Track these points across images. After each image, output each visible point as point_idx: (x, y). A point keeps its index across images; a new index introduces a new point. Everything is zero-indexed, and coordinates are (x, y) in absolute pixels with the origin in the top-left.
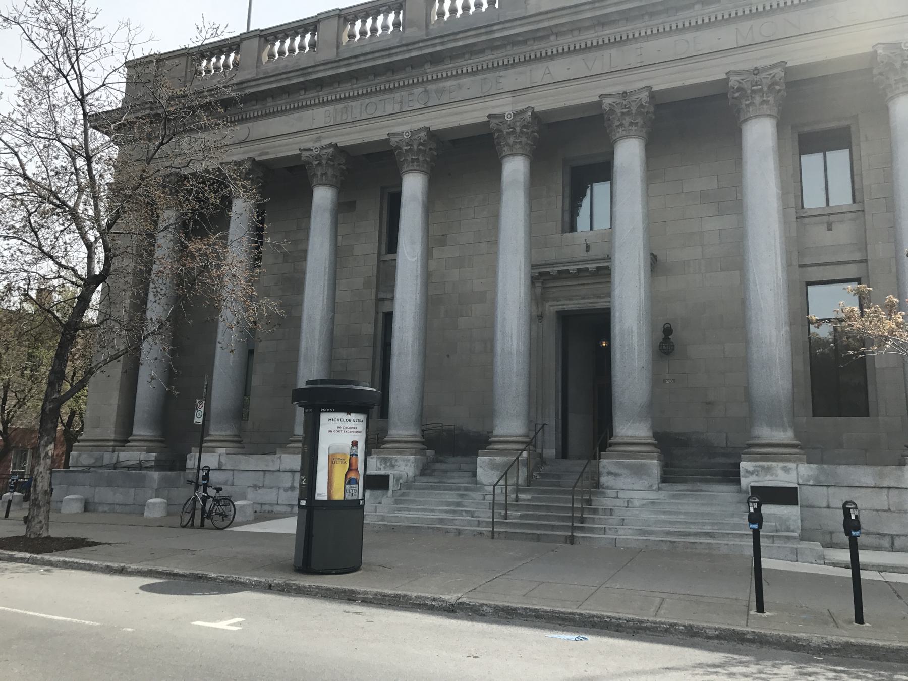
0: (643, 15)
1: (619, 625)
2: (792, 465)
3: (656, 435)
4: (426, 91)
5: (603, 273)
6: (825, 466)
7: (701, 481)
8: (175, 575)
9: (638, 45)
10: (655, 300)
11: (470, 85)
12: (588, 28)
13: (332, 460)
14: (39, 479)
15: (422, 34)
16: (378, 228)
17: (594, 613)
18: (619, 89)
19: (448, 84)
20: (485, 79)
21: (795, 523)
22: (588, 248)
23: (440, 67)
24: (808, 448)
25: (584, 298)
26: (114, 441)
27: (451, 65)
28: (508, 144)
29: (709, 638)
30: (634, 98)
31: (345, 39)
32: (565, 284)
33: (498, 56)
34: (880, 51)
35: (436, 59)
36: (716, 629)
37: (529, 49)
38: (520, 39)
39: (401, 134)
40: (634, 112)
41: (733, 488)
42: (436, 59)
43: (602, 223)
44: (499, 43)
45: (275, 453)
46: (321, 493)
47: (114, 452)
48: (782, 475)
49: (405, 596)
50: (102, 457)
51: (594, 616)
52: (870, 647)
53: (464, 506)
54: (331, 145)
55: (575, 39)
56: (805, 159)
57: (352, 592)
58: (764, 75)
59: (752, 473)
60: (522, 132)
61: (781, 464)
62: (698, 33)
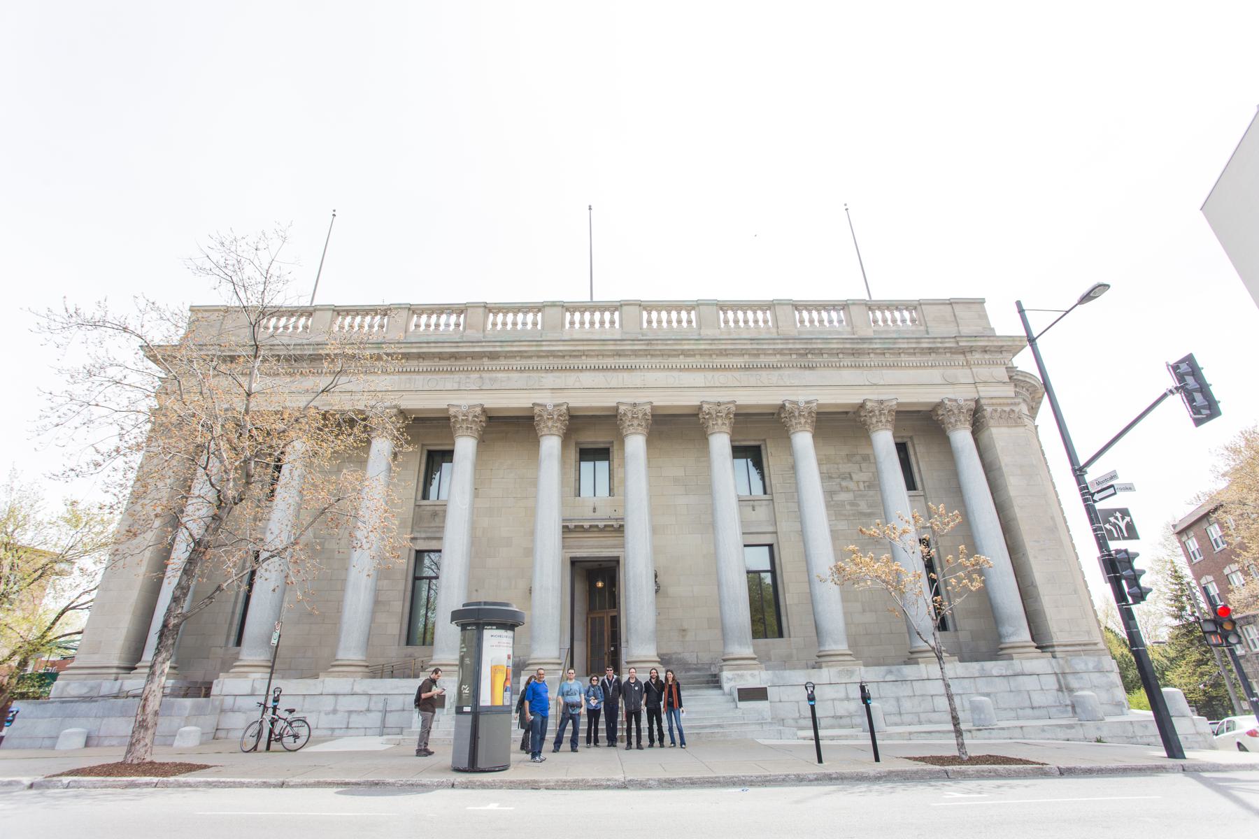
2: (756, 672)
5: (619, 530)
8: (347, 784)
10: (656, 550)
11: (517, 379)
12: (609, 356)
13: (494, 670)
14: (151, 698)
15: (479, 336)
19: (500, 375)
21: (768, 715)
24: (763, 659)
26: (118, 668)
31: (412, 328)
33: (544, 363)
35: (493, 356)
41: (719, 692)
42: (493, 356)
43: (443, 496)
45: (316, 676)
46: (485, 700)
47: (116, 679)
48: (753, 679)
50: (100, 685)
54: (395, 407)
57: (536, 782)
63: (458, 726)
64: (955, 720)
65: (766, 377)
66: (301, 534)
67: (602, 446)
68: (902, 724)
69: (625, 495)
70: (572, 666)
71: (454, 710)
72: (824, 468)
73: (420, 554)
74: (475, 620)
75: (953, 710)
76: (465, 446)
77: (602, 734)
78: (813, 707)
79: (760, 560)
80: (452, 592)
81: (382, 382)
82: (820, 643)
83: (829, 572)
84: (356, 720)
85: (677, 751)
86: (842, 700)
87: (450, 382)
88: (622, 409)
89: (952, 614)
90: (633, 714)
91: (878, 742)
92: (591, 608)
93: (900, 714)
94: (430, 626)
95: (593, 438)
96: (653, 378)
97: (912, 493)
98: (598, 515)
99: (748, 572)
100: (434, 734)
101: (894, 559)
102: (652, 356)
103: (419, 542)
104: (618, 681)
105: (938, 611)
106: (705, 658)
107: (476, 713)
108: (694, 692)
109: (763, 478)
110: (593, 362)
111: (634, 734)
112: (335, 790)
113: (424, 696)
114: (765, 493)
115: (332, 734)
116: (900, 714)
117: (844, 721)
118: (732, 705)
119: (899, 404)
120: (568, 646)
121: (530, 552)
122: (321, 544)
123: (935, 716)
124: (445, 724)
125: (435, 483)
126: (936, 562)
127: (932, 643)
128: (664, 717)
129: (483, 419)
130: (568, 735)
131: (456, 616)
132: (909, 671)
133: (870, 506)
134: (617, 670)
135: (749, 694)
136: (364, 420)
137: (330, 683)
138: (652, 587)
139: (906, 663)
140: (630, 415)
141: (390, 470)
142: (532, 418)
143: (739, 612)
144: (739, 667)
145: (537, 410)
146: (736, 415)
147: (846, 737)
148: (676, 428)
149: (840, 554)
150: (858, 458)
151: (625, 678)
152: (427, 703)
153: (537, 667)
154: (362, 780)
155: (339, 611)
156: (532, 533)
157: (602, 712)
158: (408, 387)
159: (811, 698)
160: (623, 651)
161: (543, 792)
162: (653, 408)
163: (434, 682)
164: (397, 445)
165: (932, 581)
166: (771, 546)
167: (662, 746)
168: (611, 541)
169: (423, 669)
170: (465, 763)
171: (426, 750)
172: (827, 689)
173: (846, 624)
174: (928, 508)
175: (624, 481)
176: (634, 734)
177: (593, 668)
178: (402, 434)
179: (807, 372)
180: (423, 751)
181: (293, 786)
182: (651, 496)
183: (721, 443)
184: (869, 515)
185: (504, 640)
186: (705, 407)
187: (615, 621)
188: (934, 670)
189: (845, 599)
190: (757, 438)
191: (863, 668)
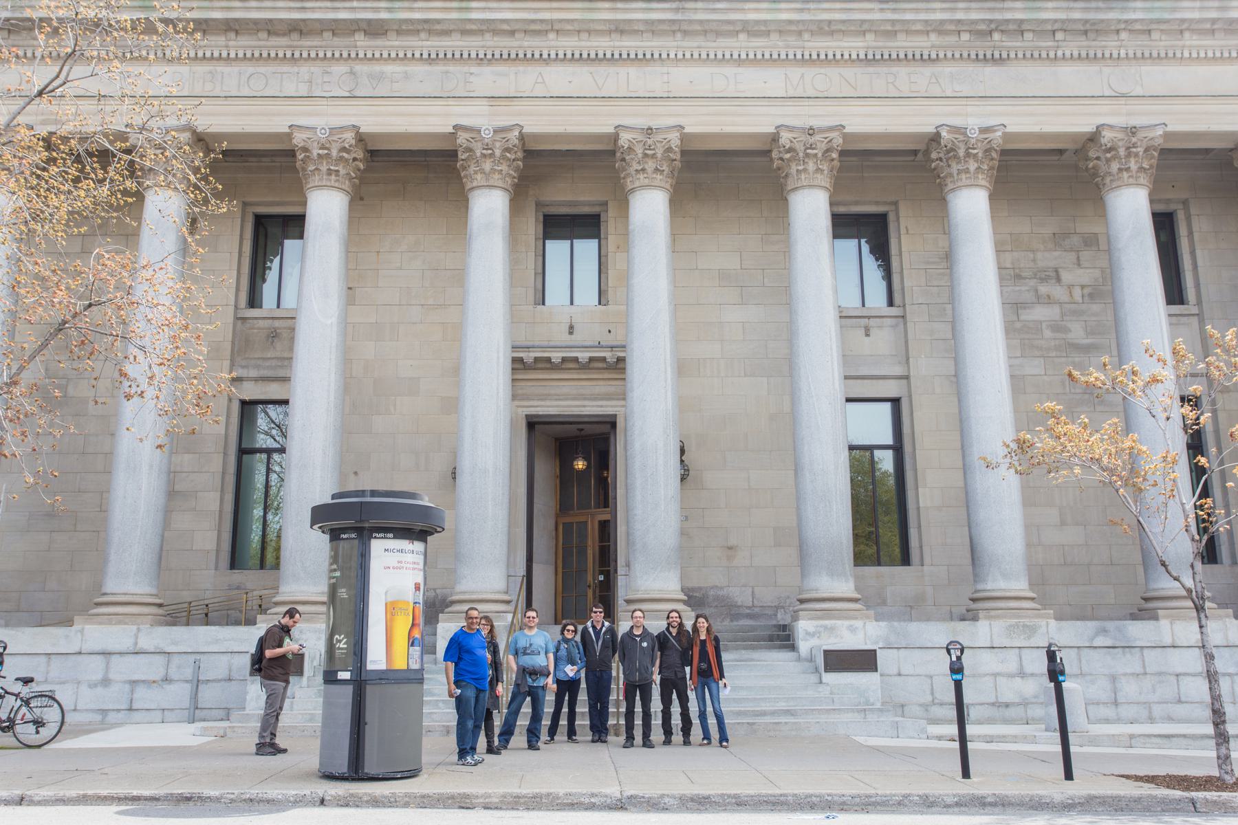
0: (674, 32)
1: (844, 803)
2: (858, 624)
3: (684, 590)
4: (352, 73)
5: (613, 366)
6: (896, 624)
7: (745, 648)
9: (665, 69)
10: (684, 406)
11: (423, 77)
13: (392, 609)
16: (235, 267)
17: (811, 792)
18: (642, 122)
19: (389, 68)
20: (447, 72)
21: (876, 696)
22: (571, 329)
23: (379, 42)
25: (567, 399)
27: (397, 43)
28: (482, 171)
29: (947, 806)
30: (660, 137)
32: (541, 376)
33: (473, 44)
34: (944, 134)
36: (954, 796)
37: (516, 44)
38: (505, 27)
39: (313, 129)
40: (659, 155)
43: (289, 301)
44: (474, 27)
45: (69, 622)
46: (376, 659)
48: (854, 634)
49: (549, 795)
51: (811, 796)
52: (1113, 798)
53: (433, 695)
55: (583, 44)
56: (550, 244)
57: (467, 796)
58: (818, 137)
59: (812, 635)
60: (503, 157)
61: (847, 623)
62: (740, 70)
63: (328, 704)
64: (1218, 717)
65: (906, 78)
66: (21, 369)
67: (586, 210)
68: (1118, 720)
69: (628, 302)
70: (529, 605)
71: (320, 678)
72: (1008, 259)
73: (248, 408)
74: (355, 521)
75: (1216, 698)
76: (326, 208)
77: (583, 722)
78: (958, 685)
79: (874, 426)
80: (310, 472)
81: (159, 78)
82: (977, 576)
83: (1002, 451)
84: (144, 697)
85: (714, 751)
86: (1011, 676)
87: (292, 80)
88: (625, 138)
89: (1230, 533)
90: (637, 688)
91: (1073, 749)
92: (564, 506)
93: (1116, 703)
94: (272, 536)
95: (568, 195)
96: (684, 78)
97: (1176, 309)
98: (579, 338)
99: (852, 448)
100: (287, 719)
101: (1128, 429)
102: (686, 33)
103: (246, 385)
104: (612, 632)
105: (1204, 525)
106: (767, 596)
107: (361, 683)
108: (745, 654)
109: (888, 277)
110: (568, 44)
111: (638, 722)
112: (115, 808)
113: (269, 653)
114: (891, 303)
115: (103, 719)
116: (1116, 703)
117: (1011, 712)
118: (813, 678)
119: (1167, 136)
120: (522, 571)
121: (452, 405)
122: (63, 388)
123: (1180, 710)
124: (306, 701)
125: (272, 276)
126: (1210, 439)
127: (1189, 583)
128: (692, 695)
129: (360, 154)
130: (523, 721)
131: (320, 515)
132: (1139, 631)
133: (1089, 333)
134: (610, 614)
135: (839, 661)
136: (128, 151)
137: (94, 634)
138: (674, 470)
139: (1134, 617)
140: (639, 150)
141: (184, 249)
142: (453, 154)
143: (832, 516)
144: (828, 614)
145: (462, 138)
146: (843, 153)
147: (1015, 739)
148: (727, 178)
149: (1026, 418)
150: (1075, 240)
151: (623, 627)
152: (273, 666)
153: (465, 607)
154: (161, 792)
155: (103, 508)
156: (456, 371)
157: (583, 685)
158: (208, 89)
159: (957, 668)
160: (621, 581)
161: (479, 815)
162: (685, 138)
163: (286, 630)
164: (194, 203)
165: (1198, 472)
166: (896, 402)
167: (687, 742)
168: (601, 388)
169: (262, 609)
170: (343, 767)
171: (273, 745)
172: (986, 656)
173: (1029, 545)
174: (1204, 338)
175: (626, 277)
176: (638, 722)
177: (567, 609)
178: (205, 178)
179: (989, 70)
180: (268, 746)
181: (39, 803)
182: (677, 306)
183: (811, 208)
184: (1087, 349)
185: (409, 558)
186: (785, 137)
187: (607, 531)
188: (1187, 631)
189: (1029, 500)
190: (883, 197)
191: (1053, 622)
